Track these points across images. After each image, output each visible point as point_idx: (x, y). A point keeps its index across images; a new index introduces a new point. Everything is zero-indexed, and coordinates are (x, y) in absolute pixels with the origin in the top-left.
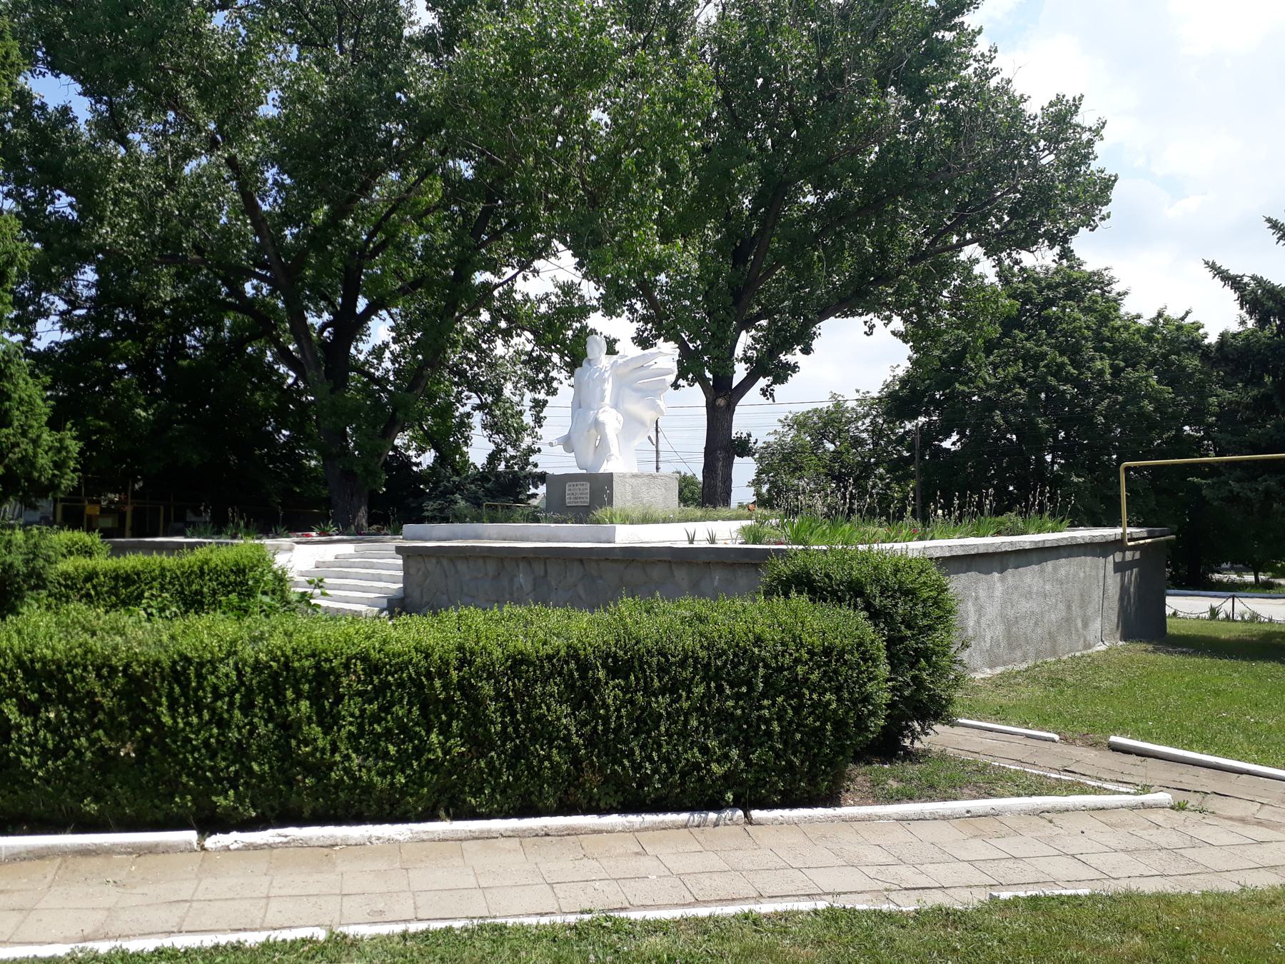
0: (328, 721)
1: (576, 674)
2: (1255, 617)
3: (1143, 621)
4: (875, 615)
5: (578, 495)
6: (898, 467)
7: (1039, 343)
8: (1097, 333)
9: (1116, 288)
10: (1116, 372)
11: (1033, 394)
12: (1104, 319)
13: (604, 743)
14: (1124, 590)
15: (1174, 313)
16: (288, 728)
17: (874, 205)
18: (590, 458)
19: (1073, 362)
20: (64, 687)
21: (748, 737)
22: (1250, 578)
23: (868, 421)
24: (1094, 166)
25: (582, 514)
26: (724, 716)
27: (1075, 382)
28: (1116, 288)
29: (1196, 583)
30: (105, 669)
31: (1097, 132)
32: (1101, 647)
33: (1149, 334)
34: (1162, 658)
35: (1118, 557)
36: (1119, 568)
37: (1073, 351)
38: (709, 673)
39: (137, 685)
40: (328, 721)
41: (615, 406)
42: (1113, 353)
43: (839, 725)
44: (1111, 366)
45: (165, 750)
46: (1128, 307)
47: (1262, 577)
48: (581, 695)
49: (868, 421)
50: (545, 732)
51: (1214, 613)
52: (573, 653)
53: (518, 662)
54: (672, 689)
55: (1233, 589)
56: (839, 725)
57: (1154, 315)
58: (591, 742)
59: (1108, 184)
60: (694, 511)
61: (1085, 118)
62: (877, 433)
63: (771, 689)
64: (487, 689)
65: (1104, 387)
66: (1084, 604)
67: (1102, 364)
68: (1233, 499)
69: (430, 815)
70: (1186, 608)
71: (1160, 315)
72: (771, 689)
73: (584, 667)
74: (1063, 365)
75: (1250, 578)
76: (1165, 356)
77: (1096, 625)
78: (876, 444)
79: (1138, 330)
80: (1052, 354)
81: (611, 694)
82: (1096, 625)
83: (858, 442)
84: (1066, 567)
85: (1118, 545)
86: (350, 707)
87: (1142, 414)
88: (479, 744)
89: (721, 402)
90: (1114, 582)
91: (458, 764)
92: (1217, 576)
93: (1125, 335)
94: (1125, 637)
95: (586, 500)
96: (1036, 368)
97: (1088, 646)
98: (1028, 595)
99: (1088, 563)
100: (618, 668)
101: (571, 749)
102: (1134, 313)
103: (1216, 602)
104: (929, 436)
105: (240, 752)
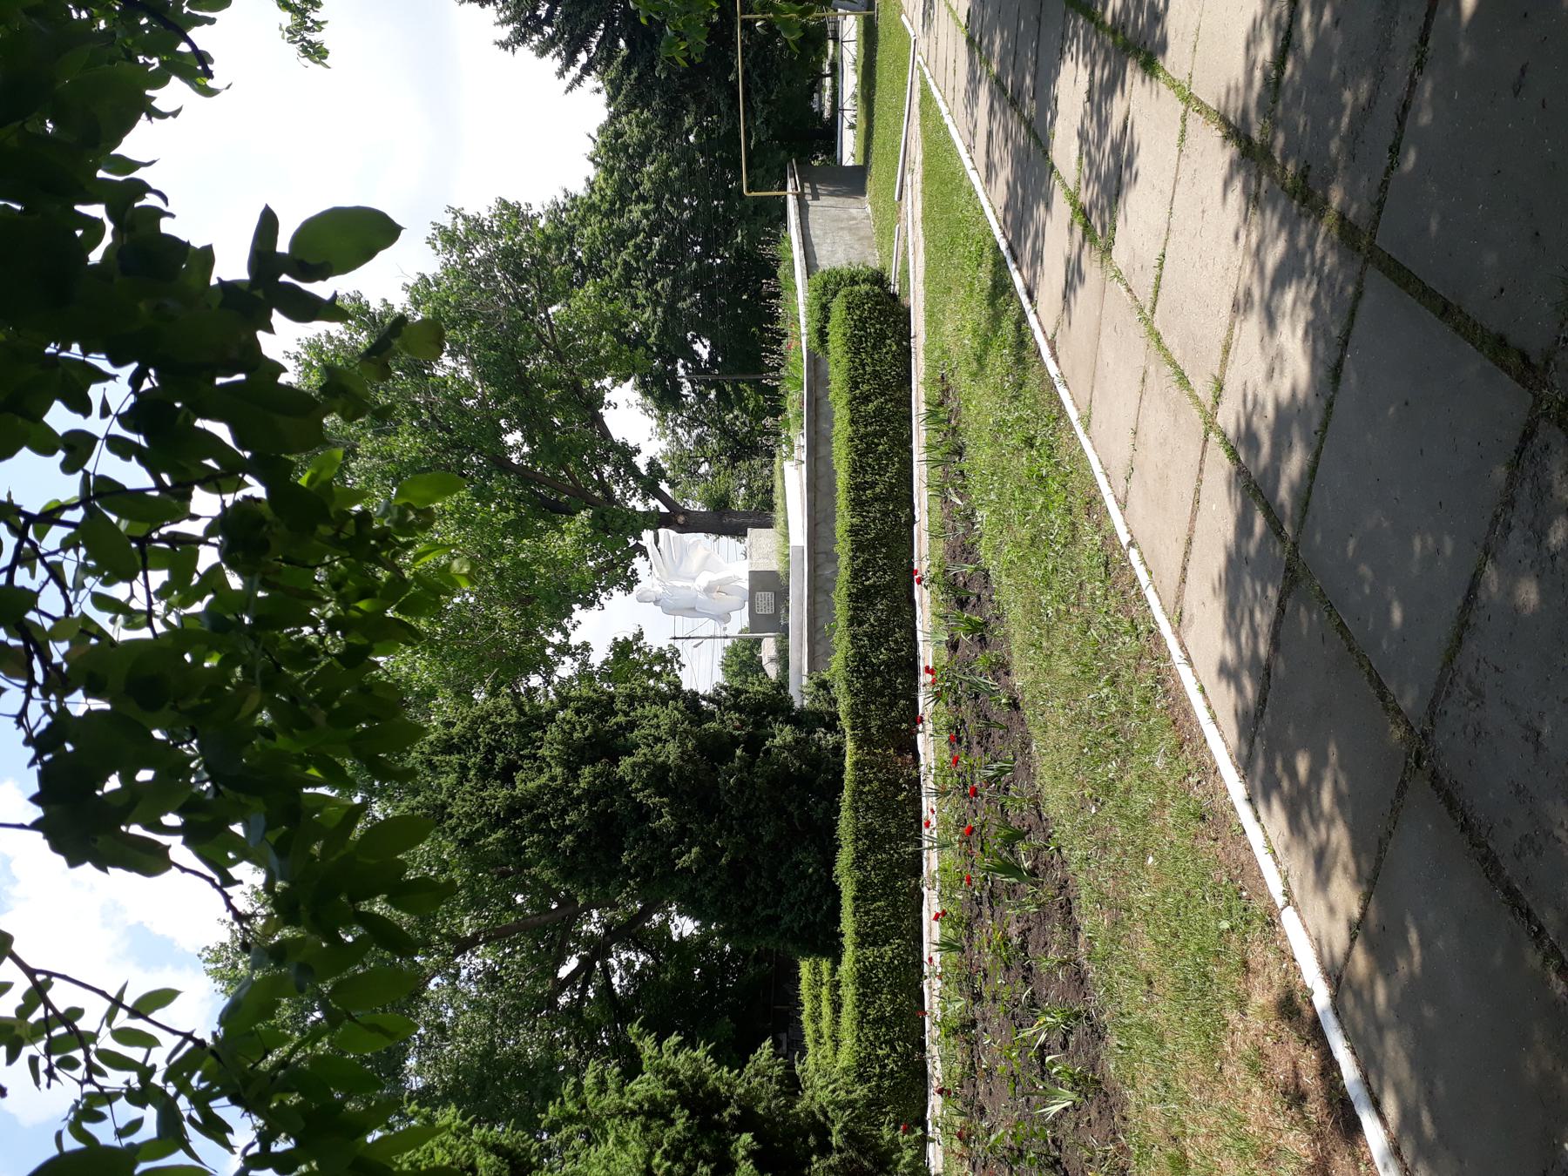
0: (873, 485)
1: (858, 401)
2: (854, 96)
3: (853, 182)
4: (835, 294)
5: (766, 601)
6: (725, 401)
7: (614, 266)
8: (607, 214)
9: (561, 199)
10: (643, 199)
11: (663, 273)
12: (592, 208)
13: (884, 389)
14: (832, 194)
15: (590, 148)
16: (876, 498)
17: (523, 384)
18: (735, 599)
19: (631, 237)
20: (860, 570)
21: (882, 337)
22: (828, 81)
23: (679, 430)
24: (485, 214)
25: (782, 595)
26: (874, 347)
27: (651, 233)
28: (561, 199)
29: (828, 136)
30: (853, 559)
31: (457, 213)
32: (869, 209)
33: (610, 171)
34: (873, 171)
35: (808, 198)
36: (816, 197)
37: (621, 237)
38: (857, 353)
39: (858, 548)
40: (873, 485)
41: (694, 579)
42: (625, 201)
43: (877, 303)
44: (637, 203)
45: (886, 536)
46: (580, 189)
47: (827, 70)
48: (866, 399)
49: (679, 430)
50: (879, 410)
51: (852, 126)
52: (850, 402)
53: (853, 422)
54: (863, 366)
55: (836, 108)
56: (877, 303)
57: (591, 164)
58: (882, 395)
59: (504, 204)
60: (778, 516)
61: (447, 221)
62: (693, 422)
63: (864, 329)
64: (862, 430)
65: (656, 210)
66: (838, 219)
67: (636, 212)
68: (767, 122)
69: (911, 452)
70: (849, 149)
71: (592, 160)
72: (864, 329)
73: (855, 398)
74: (636, 245)
75: (828, 81)
76: (630, 157)
77: (854, 211)
78: (702, 424)
79: (605, 180)
80: (624, 255)
81: (866, 387)
82: (854, 211)
83: (700, 441)
84: (815, 231)
85: (800, 198)
86: (868, 478)
87: (680, 178)
88: (884, 433)
89: (681, 519)
90: (825, 201)
91: (891, 439)
92: (826, 114)
93: (609, 192)
94: (864, 194)
95: (770, 595)
96: (638, 270)
97: (868, 217)
98: (834, 252)
99: (812, 216)
100: (855, 385)
101: (886, 402)
102: (584, 184)
103: (846, 124)
104: (698, 371)
105: (885, 514)
